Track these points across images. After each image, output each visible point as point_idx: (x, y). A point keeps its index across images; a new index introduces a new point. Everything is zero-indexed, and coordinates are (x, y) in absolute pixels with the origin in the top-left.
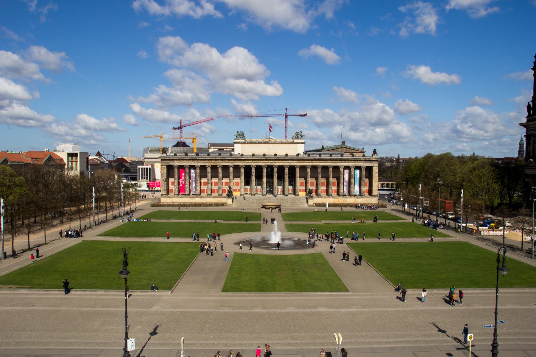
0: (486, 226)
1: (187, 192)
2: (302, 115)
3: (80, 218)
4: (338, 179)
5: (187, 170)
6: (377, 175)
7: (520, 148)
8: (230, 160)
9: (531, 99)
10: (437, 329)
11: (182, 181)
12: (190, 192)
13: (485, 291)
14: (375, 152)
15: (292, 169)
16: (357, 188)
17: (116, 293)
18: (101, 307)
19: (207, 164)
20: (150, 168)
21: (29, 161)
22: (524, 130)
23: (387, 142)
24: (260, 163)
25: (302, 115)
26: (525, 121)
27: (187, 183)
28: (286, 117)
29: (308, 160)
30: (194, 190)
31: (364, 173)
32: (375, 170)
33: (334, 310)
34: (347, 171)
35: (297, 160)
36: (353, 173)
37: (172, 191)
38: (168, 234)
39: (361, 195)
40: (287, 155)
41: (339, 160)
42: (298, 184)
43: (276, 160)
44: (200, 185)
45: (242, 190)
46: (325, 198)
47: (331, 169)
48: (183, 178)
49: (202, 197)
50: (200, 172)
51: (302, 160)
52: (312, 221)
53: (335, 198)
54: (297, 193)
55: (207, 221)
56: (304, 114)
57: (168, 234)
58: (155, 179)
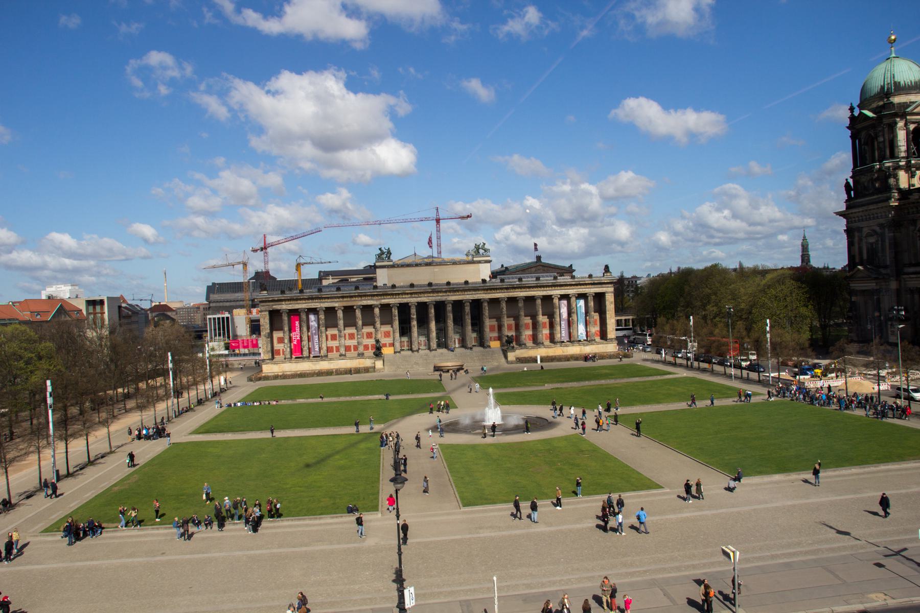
0: (807, 374)
1: (306, 353)
3: (141, 408)
4: (551, 316)
5: (304, 316)
6: (613, 306)
7: (803, 251)
8: (374, 296)
9: (851, 174)
10: (834, 531)
12: (310, 353)
13: (867, 470)
14: (607, 269)
15: (477, 305)
16: (581, 329)
17: (290, 523)
18: (280, 547)
19: (336, 305)
20: (228, 318)
21: (26, 316)
22: (844, 221)
23: (588, 253)
24: (424, 299)
26: (842, 207)
27: (305, 338)
28: (438, 221)
29: (502, 289)
30: (317, 349)
31: (591, 304)
32: (610, 299)
33: (658, 518)
34: (564, 302)
35: (484, 290)
36: (574, 306)
37: (278, 352)
38: (692, 396)
39: (589, 340)
40: (466, 282)
41: (551, 286)
42: (487, 329)
43: (450, 291)
44: (327, 339)
45: (397, 345)
46: (533, 348)
47: (539, 302)
48: (298, 329)
49: (331, 359)
50: (325, 318)
51: (491, 289)
52: (529, 386)
53: (548, 347)
54: (486, 344)
55: (357, 398)
56: (465, 214)
57: (692, 396)
58: (235, 336)
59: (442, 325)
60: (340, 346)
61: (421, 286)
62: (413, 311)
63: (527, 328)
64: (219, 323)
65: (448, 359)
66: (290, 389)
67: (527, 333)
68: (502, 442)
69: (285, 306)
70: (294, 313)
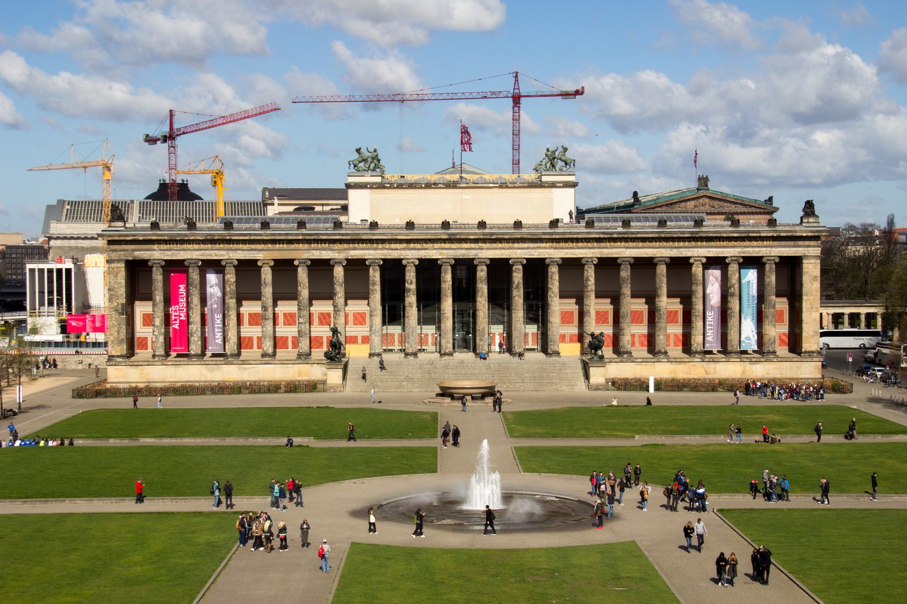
1: (195, 348)
2: (566, 95)
4: (687, 300)
5: (194, 275)
6: (817, 285)
8: (334, 241)
11: (178, 312)
14: (809, 209)
15: (536, 270)
19: (259, 256)
20: (68, 271)
23: (852, 174)
24: (432, 252)
25: (566, 95)
27: (196, 318)
28: (517, 99)
32: (811, 271)
35: (552, 240)
36: (734, 280)
37: (143, 343)
39: (763, 350)
40: (518, 225)
41: (689, 239)
43: (484, 241)
45: (376, 340)
46: (644, 361)
47: (662, 269)
48: (183, 301)
49: (244, 362)
50: (238, 282)
52: (603, 436)
53: (676, 361)
54: (552, 348)
55: (260, 441)
56: (572, 88)
58: (86, 307)
59: (464, 305)
60: (264, 336)
61: (428, 227)
62: (411, 275)
63: (780, 319)
64: (50, 282)
65: (465, 370)
66: (139, 414)
67: (635, 331)
68: (496, 546)
69: (157, 254)
70: (175, 268)
